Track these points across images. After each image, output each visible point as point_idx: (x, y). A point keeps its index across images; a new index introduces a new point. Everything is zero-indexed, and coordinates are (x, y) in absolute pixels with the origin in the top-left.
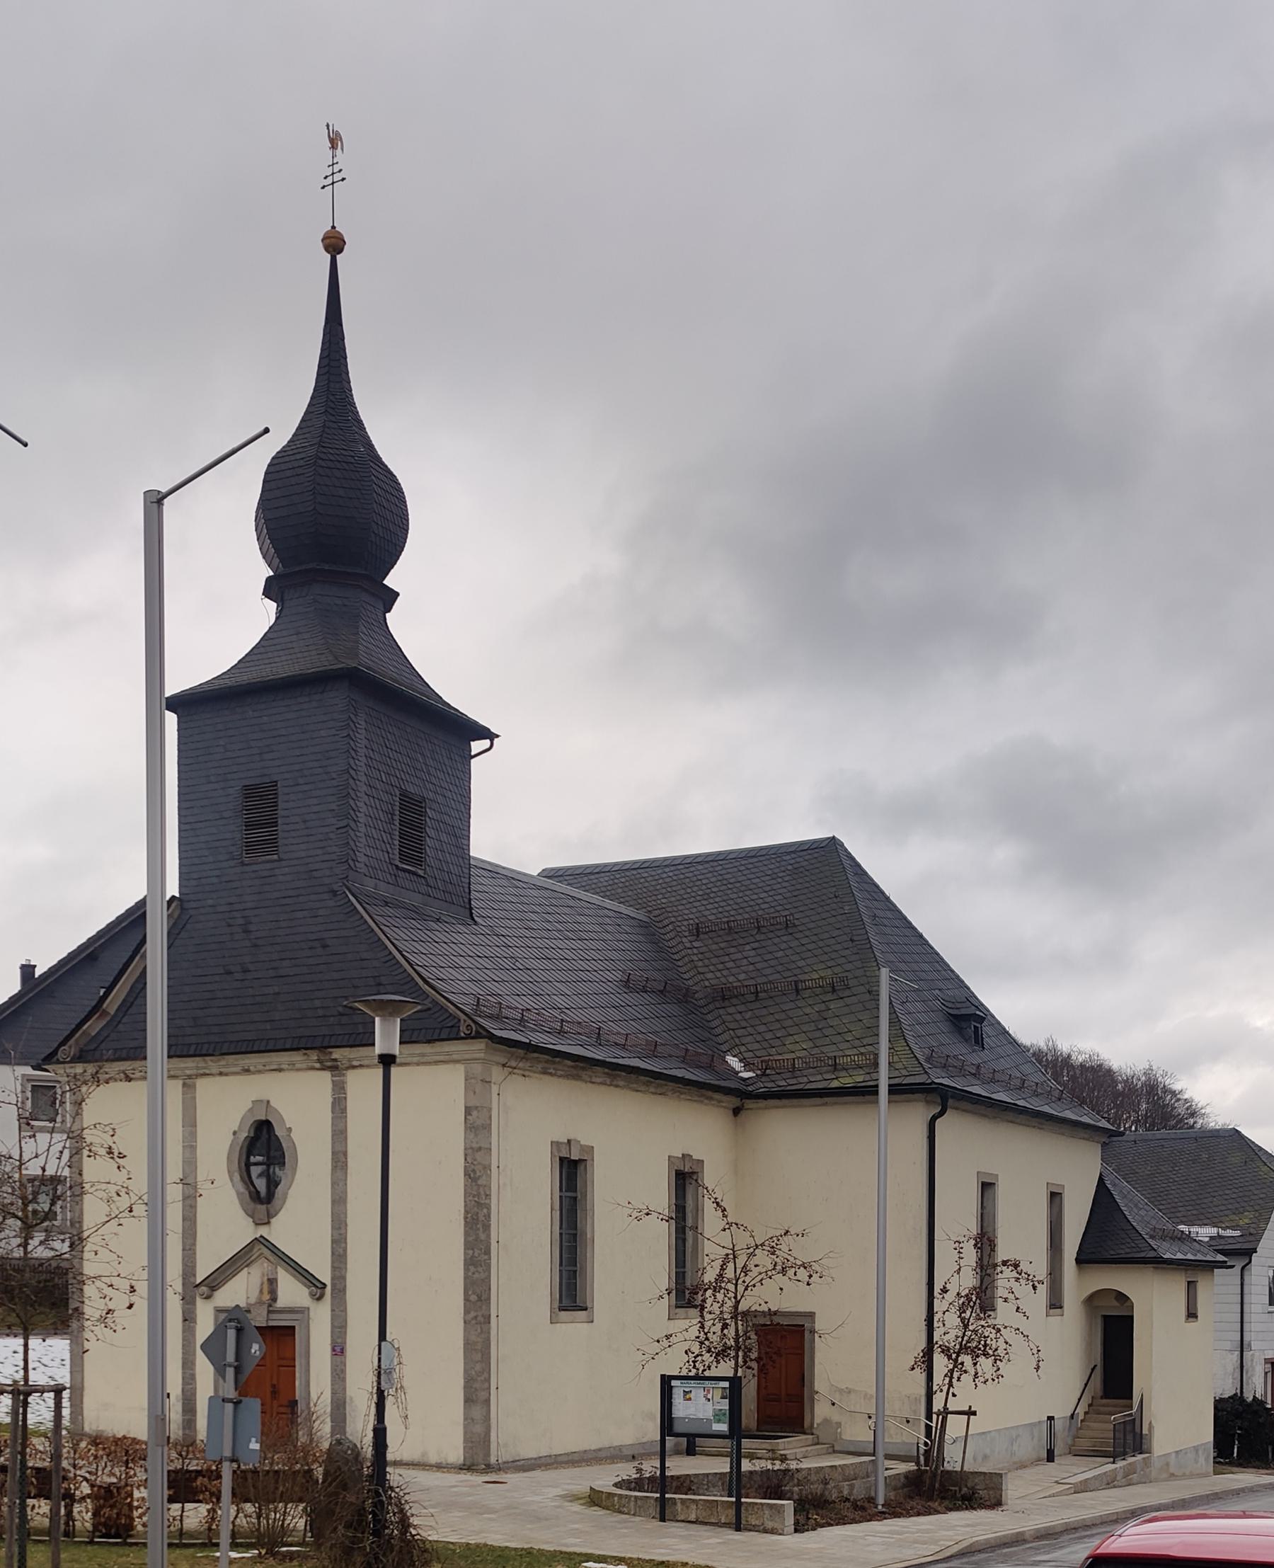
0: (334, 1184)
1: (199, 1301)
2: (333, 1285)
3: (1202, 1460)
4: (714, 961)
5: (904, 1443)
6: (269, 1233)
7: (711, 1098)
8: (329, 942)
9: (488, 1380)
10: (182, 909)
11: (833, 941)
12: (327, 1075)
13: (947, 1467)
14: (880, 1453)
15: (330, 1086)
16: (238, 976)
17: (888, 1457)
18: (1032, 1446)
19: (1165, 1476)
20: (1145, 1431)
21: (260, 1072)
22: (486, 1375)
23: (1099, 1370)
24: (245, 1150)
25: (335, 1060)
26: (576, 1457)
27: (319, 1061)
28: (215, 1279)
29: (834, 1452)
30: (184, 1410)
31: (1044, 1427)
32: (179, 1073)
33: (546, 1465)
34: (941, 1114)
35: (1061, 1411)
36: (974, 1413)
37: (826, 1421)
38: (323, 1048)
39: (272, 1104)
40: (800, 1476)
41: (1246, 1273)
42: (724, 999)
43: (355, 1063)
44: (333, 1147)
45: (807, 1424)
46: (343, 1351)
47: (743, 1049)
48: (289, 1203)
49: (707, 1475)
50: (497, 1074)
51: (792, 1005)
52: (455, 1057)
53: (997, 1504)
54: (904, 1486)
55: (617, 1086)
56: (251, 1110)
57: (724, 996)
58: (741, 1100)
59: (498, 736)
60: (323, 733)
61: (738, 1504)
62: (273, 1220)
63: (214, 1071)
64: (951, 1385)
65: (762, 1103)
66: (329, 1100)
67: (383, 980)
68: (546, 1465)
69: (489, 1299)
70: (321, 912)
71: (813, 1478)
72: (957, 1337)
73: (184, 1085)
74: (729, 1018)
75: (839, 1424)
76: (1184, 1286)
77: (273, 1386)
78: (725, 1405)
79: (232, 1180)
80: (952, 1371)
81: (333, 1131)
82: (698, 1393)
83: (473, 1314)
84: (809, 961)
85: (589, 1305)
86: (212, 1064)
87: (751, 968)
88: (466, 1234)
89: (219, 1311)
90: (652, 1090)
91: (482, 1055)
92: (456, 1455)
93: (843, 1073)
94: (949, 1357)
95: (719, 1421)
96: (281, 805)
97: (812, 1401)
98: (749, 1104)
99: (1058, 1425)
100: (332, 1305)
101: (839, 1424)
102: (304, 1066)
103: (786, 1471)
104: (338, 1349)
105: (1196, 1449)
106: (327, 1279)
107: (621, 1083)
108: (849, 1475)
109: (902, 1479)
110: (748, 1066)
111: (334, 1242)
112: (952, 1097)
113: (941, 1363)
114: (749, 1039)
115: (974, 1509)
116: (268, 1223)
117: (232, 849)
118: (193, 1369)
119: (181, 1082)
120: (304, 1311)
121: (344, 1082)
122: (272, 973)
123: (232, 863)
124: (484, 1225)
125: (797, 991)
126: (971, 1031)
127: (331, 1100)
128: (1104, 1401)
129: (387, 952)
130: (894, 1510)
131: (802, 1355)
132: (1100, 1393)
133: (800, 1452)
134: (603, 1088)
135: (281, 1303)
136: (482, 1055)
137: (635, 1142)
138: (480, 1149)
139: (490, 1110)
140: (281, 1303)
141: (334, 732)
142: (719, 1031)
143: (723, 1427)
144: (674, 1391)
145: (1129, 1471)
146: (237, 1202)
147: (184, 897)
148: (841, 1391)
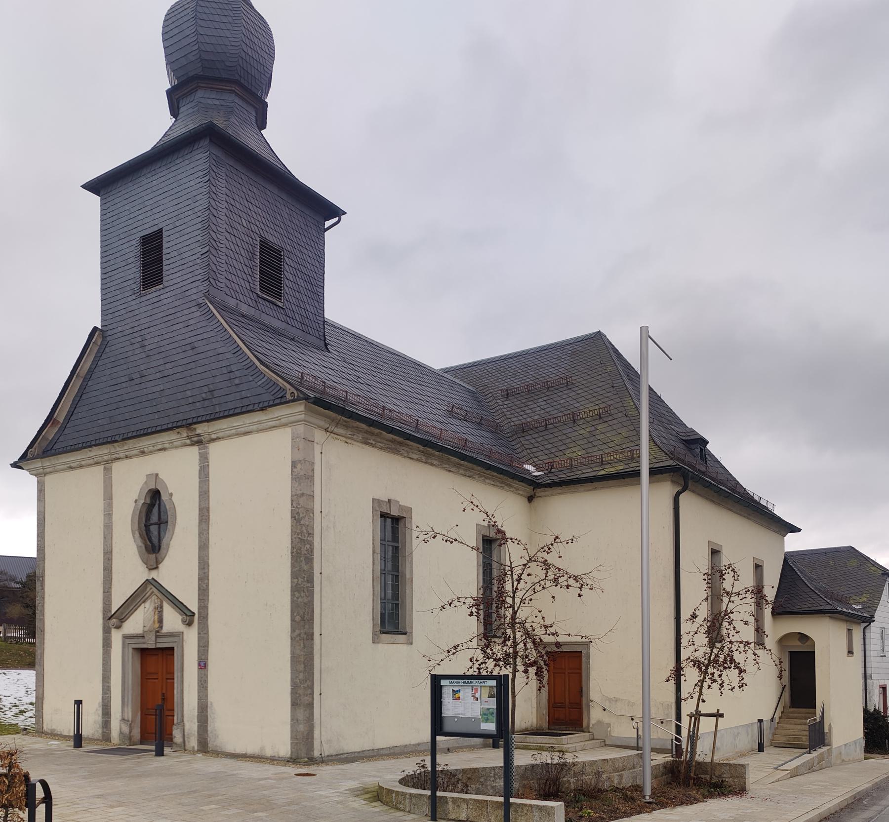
0: (200, 534)
1: (113, 631)
2: (199, 613)
3: (858, 750)
4: (519, 410)
5: (659, 739)
6: (158, 576)
7: (510, 486)
8: (196, 345)
9: (311, 687)
10: (104, 338)
11: (599, 389)
12: (195, 450)
13: (698, 758)
14: (647, 749)
15: (198, 457)
16: (137, 381)
17: (653, 750)
18: (748, 740)
19: (839, 761)
20: (826, 730)
21: (151, 452)
22: (309, 683)
23: (787, 689)
24: (144, 514)
25: (199, 435)
26: (397, 750)
27: (189, 437)
28: (122, 613)
29: (606, 745)
30: (103, 714)
31: (756, 727)
32: (100, 459)
33: (369, 757)
34: (683, 490)
35: (766, 717)
36: (722, 716)
37: (599, 722)
38: (189, 425)
39: (160, 476)
40: (576, 769)
41: (867, 631)
42: (523, 432)
43: (214, 436)
44: (200, 505)
45: (585, 724)
46: (205, 666)
47: (536, 460)
48: (171, 552)
49: (494, 768)
50: (319, 435)
51: (571, 430)
52: (283, 421)
53: (741, 791)
54: (663, 774)
55: (432, 464)
56: (146, 482)
57: (523, 429)
58: (534, 489)
59: (345, 213)
60: (192, 183)
61: (507, 805)
62: (160, 566)
63: (122, 455)
64: (701, 694)
65: (549, 491)
66: (197, 468)
67: (234, 368)
68: (369, 757)
69: (312, 619)
70: (191, 322)
71: (588, 770)
72: (705, 654)
73: (105, 469)
74: (526, 442)
75: (609, 725)
76: (845, 631)
77: (163, 694)
78: (492, 704)
79: (134, 537)
80: (702, 682)
81: (200, 492)
82: (466, 693)
83: (297, 632)
84: (582, 403)
85: (408, 630)
86: (119, 449)
87: (543, 411)
88: (293, 566)
89: (126, 637)
90: (462, 472)
91: (303, 416)
92: (284, 749)
93: (609, 466)
94: (700, 668)
95: (487, 720)
96: (165, 245)
97: (588, 707)
98: (539, 492)
99: (766, 725)
100: (199, 629)
101: (609, 725)
102: (179, 443)
103: (564, 765)
104: (202, 664)
105: (855, 742)
106: (195, 609)
107: (435, 462)
108: (618, 767)
109: (662, 769)
110: (538, 470)
111: (200, 579)
112: (692, 478)
113: (691, 675)
114: (540, 453)
115: (725, 795)
116: (157, 568)
117: (134, 286)
118: (109, 682)
119: (102, 467)
120: (179, 635)
121: (207, 453)
122: (159, 375)
123: (134, 297)
124: (306, 558)
125: (574, 421)
126: (698, 451)
127: (198, 468)
128: (792, 710)
129: (235, 345)
130: (661, 801)
131: (580, 674)
132: (788, 704)
133: (579, 746)
134: (421, 465)
135: (166, 629)
136: (303, 416)
137: (449, 510)
138: (303, 494)
139: (313, 464)
140: (166, 629)
141: (199, 180)
142: (520, 450)
143: (490, 727)
144: (444, 690)
145: (821, 758)
146: (137, 553)
147: (105, 329)
148: (610, 700)
